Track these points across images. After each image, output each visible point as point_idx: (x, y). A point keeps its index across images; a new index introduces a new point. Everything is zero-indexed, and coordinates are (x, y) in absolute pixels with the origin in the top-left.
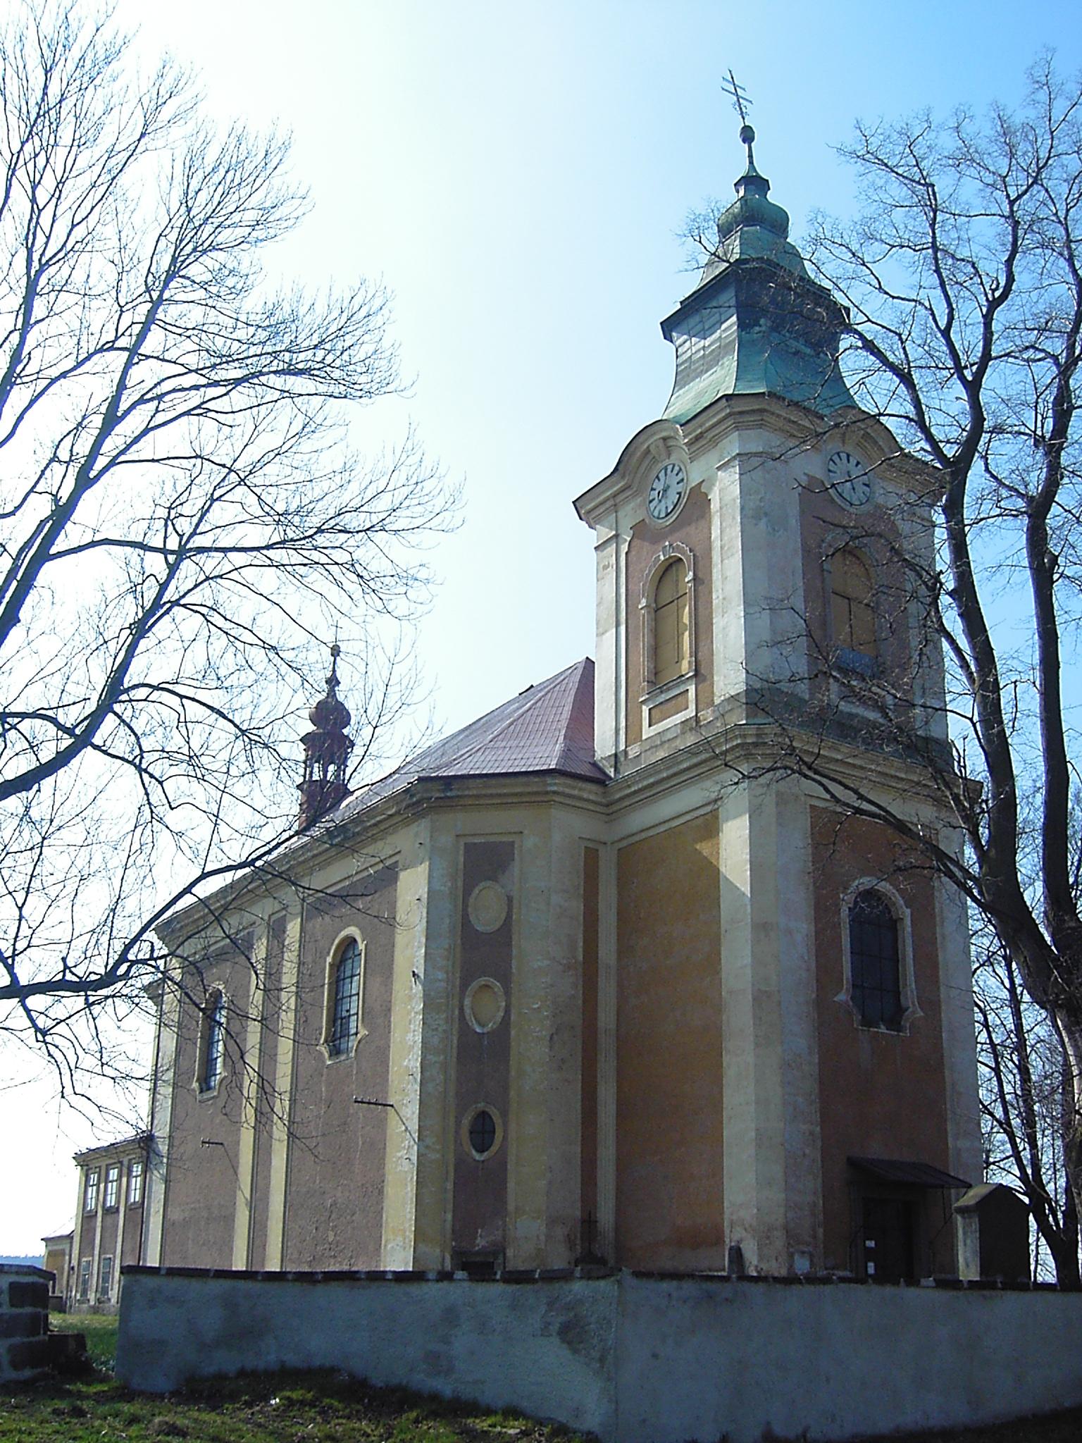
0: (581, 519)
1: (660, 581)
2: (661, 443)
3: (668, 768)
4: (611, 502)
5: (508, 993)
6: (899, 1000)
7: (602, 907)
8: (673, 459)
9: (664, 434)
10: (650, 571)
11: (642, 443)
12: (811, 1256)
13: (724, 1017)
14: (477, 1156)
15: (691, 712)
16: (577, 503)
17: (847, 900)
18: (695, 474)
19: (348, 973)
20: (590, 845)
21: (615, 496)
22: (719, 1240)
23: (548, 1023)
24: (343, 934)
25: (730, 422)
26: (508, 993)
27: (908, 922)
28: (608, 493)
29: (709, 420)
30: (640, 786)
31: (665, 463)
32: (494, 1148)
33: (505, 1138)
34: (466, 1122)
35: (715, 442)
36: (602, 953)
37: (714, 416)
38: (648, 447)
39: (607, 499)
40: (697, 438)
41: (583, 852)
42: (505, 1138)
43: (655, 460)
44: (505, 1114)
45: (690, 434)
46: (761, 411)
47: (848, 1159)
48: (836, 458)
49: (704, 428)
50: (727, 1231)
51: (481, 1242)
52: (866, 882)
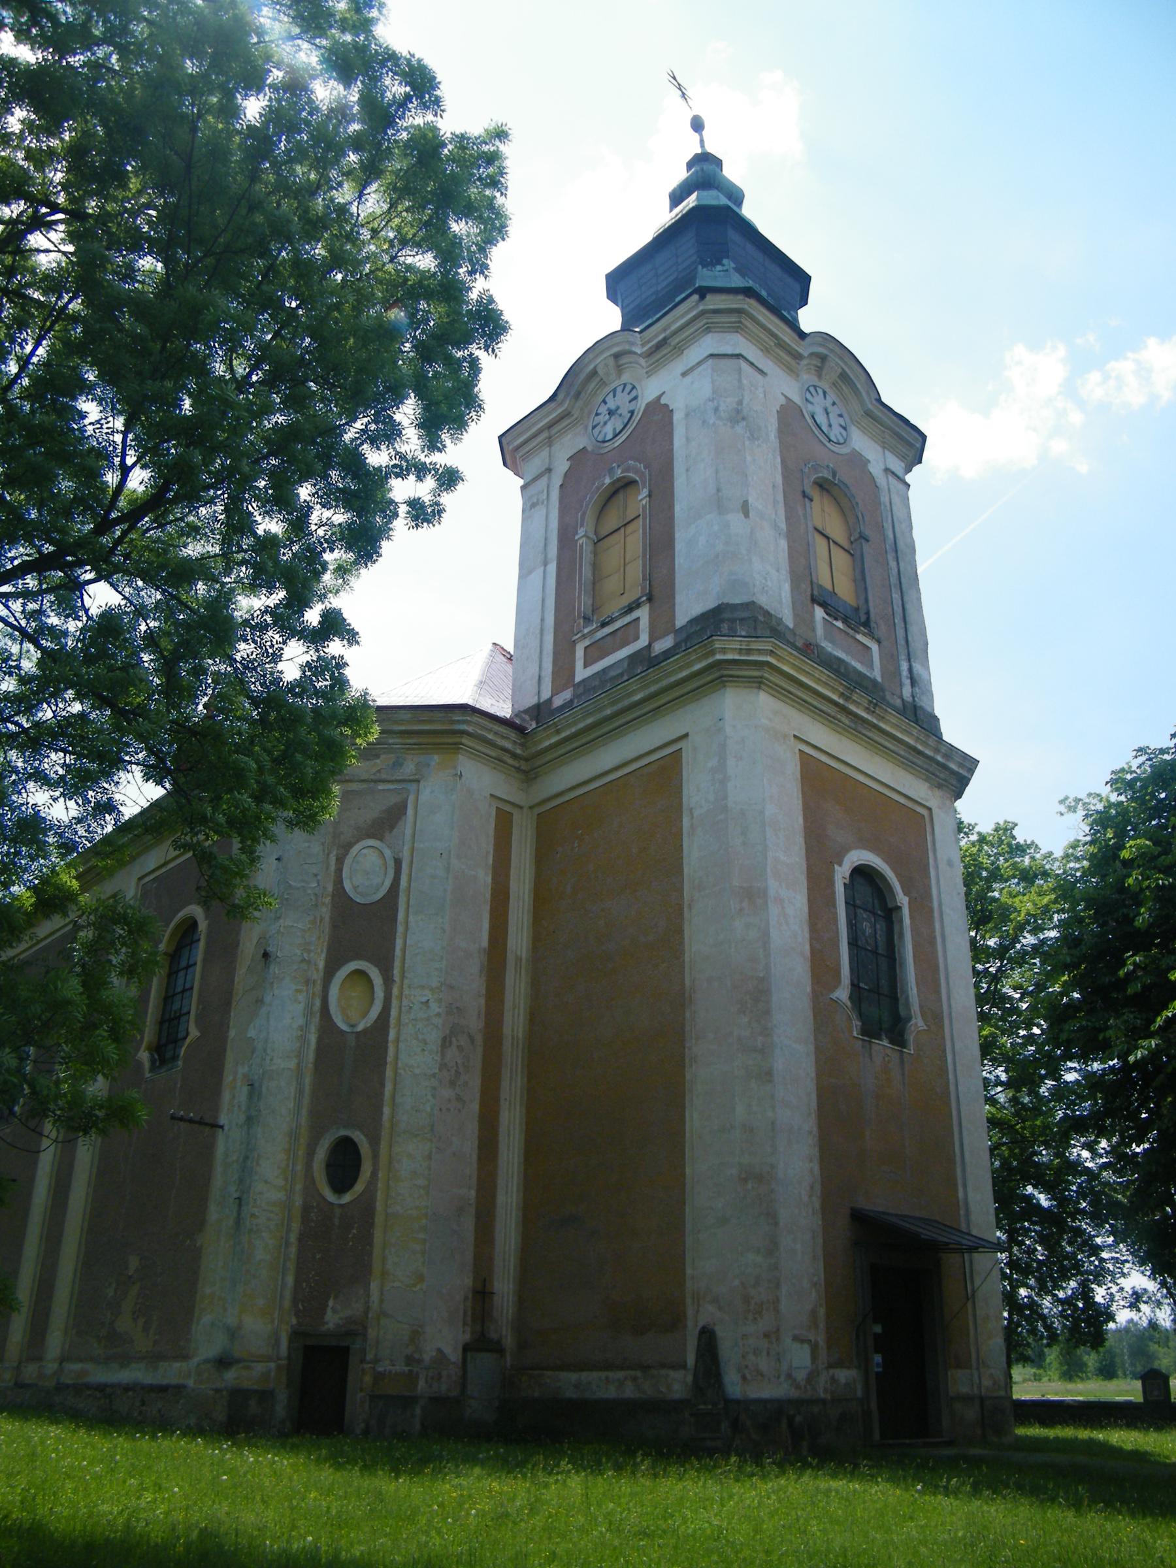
0: (505, 464)
1: (601, 512)
2: (611, 362)
3: (613, 703)
4: (545, 435)
5: (388, 981)
6: (897, 1009)
7: (513, 886)
8: (626, 378)
9: (615, 350)
10: (591, 498)
11: (590, 362)
12: (814, 1348)
13: (688, 1015)
14: (330, 1196)
15: (643, 641)
16: (503, 439)
17: (842, 873)
18: (650, 390)
19: (183, 964)
20: (508, 808)
21: (550, 426)
22: (676, 1322)
23: (438, 1021)
24: (181, 915)
25: (702, 322)
26: (388, 981)
27: (906, 911)
28: (542, 424)
29: (674, 322)
30: (573, 730)
31: (613, 386)
32: (359, 1187)
33: (374, 1174)
34: (321, 1154)
35: (679, 350)
36: (512, 942)
37: (682, 316)
38: (595, 367)
39: (540, 432)
40: (659, 346)
41: (494, 813)
42: (374, 1174)
43: (603, 383)
44: (375, 1141)
45: (649, 342)
46: (739, 311)
47: (852, 1209)
48: (812, 389)
49: (668, 332)
50: (690, 1312)
51: (333, 1319)
52: (860, 856)
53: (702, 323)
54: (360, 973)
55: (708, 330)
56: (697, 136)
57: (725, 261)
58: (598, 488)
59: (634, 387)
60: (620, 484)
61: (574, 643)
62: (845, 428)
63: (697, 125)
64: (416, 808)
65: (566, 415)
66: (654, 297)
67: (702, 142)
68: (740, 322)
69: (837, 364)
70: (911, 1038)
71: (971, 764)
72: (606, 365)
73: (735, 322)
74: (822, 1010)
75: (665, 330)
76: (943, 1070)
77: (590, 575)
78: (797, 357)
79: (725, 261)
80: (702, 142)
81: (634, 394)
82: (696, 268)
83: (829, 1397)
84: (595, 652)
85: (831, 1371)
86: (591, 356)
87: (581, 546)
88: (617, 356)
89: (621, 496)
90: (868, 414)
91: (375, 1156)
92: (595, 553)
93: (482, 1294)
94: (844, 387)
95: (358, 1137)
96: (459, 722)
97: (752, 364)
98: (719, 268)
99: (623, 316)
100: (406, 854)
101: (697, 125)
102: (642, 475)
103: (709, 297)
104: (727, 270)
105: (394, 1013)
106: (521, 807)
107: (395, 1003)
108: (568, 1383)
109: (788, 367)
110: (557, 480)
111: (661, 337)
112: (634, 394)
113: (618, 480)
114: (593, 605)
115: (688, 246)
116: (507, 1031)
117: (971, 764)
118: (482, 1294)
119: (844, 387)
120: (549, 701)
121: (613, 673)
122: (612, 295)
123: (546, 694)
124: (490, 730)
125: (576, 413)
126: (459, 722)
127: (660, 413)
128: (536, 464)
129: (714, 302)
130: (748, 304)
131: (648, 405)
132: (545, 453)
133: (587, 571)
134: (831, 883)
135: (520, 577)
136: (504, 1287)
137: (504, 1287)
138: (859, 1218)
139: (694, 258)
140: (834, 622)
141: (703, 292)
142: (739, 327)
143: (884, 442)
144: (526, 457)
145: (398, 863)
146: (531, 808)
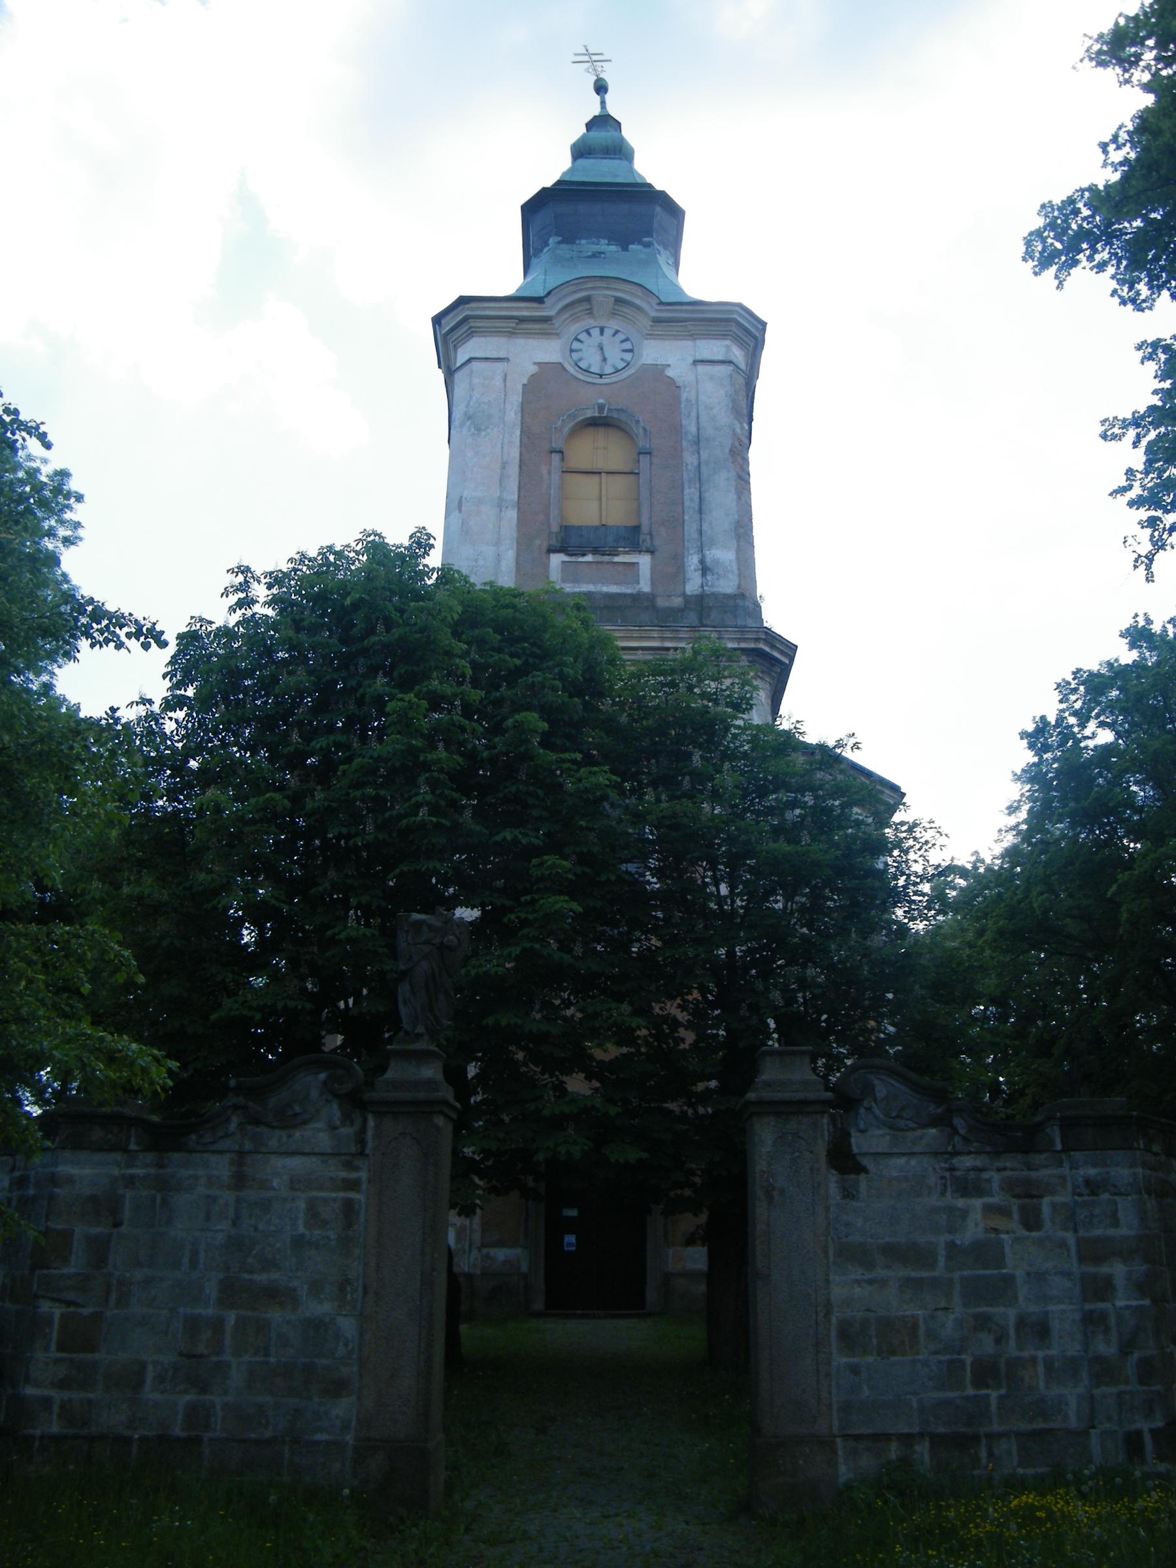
3: (739, 640)
46: (466, 319)
55: (456, 348)
56: (598, 98)
63: (601, 88)
67: (603, 103)
69: (606, 296)
71: (793, 648)
78: (546, 320)
80: (603, 103)
83: (478, 1272)
85: (485, 1251)
90: (657, 321)
94: (626, 310)
97: (486, 359)
101: (601, 88)
103: (443, 322)
109: (542, 334)
117: (793, 648)
119: (626, 310)
130: (468, 309)
140: (616, 559)
142: (472, 332)
143: (692, 335)
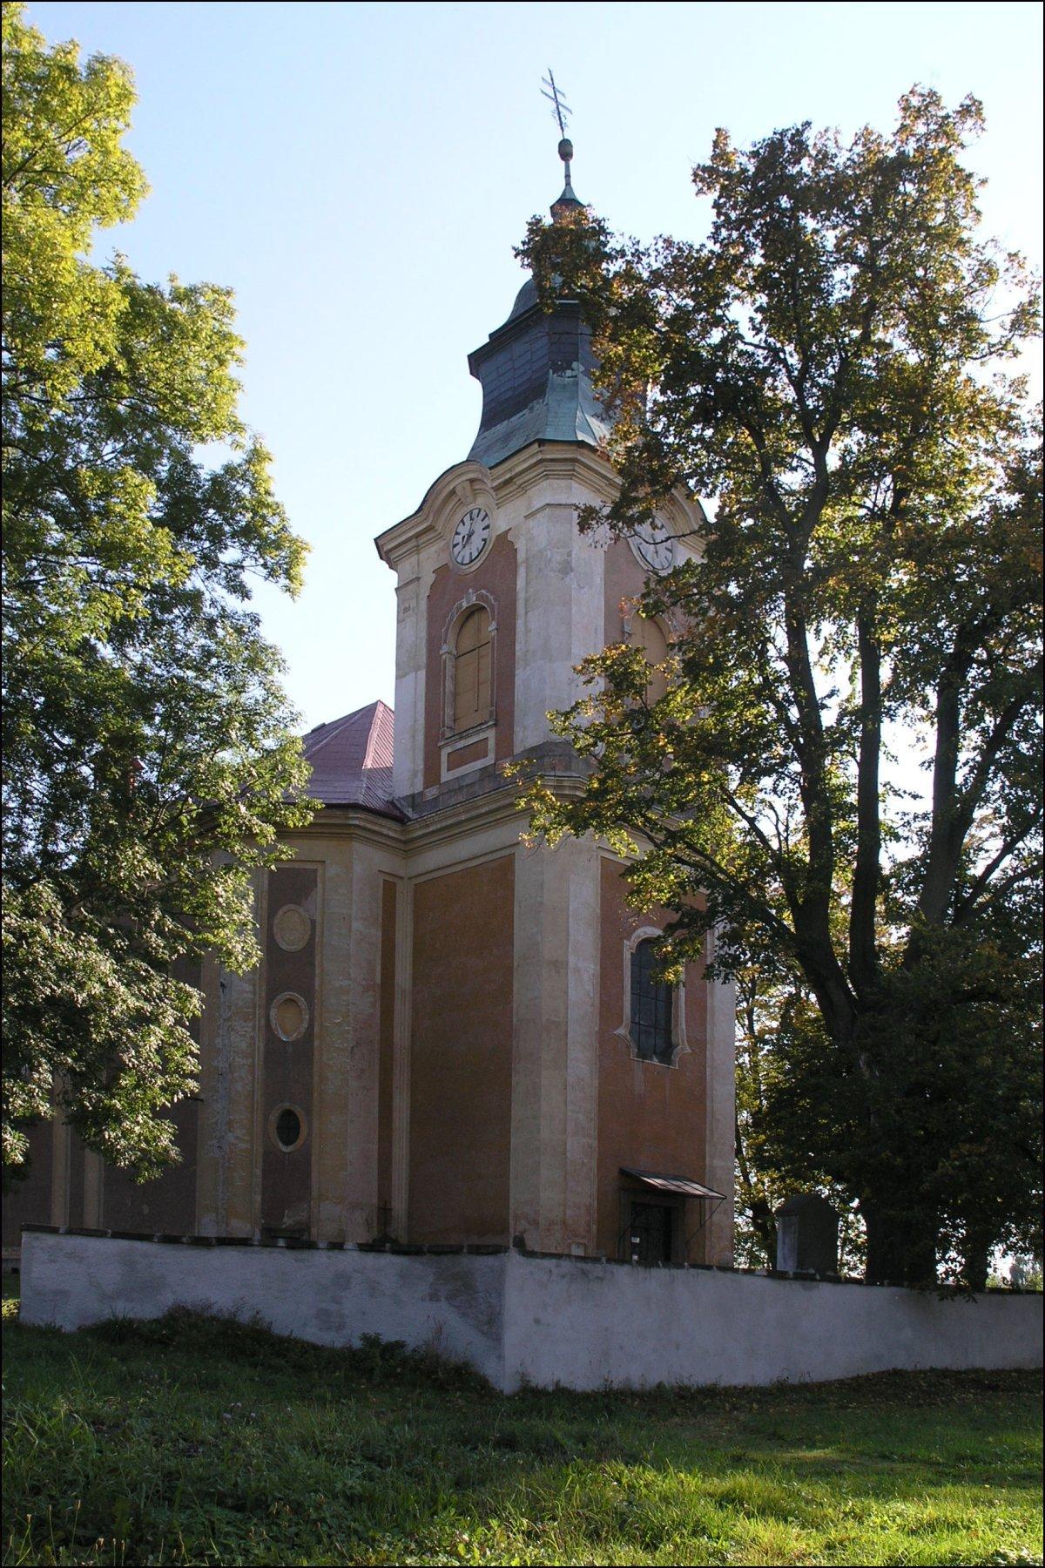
0: (381, 558)
1: (462, 626)
2: (467, 484)
3: (467, 812)
4: (413, 543)
9: (471, 476)
15: (490, 760)
17: (629, 947)
18: (502, 520)
21: (418, 536)
31: (471, 507)
32: (299, 1142)
35: (523, 489)
37: (524, 461)
44: (309, 1112)
45: (498, 478)
50: (512, 1223)
53: (540, 471)
54: (291, 1000)
56: (563, 163)
57: (575, 365)
58: (458, 609)
59: (486, 515)
60: (475, 608)
61: (440, 748)
62: (671, 551)
64: (324, 883)
65: (430, 528)
66: (510, 394)
68: (574, 470)
70: (676, 1058)
72: (464, 489)
73: (569, 470)
74: (604, 1039)
75: (510, 470)
76: (702, 1079)
77: (452, 688)
79: (575, 365)
81: (486, 522)
82: (547, 372)
84: (457, 760)
86: (449, 478)
87: (445, 661)
88: (472, 481)
89: (476, 617)
91: (310, 1122)
92: (456, 667)
93: (384, 1211)
95: (298, 1110)
96: (352, 818)
98: (569, 373)
99: (485, 405)
100: (318, 918)
102: (492, 607)
104: (576, 376)
105: (316, 1029)
106: (402, 878)
107: (317, 1025)
108: (378, 979)
110: (425, 591)
111: (508, 476)
112: (486, 522)
113: (474, 605)
114: (454, 714)
115: (536, 344)
116: (397, 1040)
118: (384, 1211)
120: (421, 794)
121: (468, 781)
122: (475, 371)
123: (419, 787)
124: (376, 824)
125: (439, 527)
126: (352, 818)
127: (503, 549)
128: (408, 564)
129: (551, 453)
131: (498, 536)
132: (414, 559)
133: (449, 685)
134: (620, 953)
135: (398, 677)
136: (399, 1204)
137: (399, 1204)
138: (623, 1173)
139: (545, 361)
141: (542, 442)
144: (401, 558)
145: (313, 922)
146: (410, 878)
